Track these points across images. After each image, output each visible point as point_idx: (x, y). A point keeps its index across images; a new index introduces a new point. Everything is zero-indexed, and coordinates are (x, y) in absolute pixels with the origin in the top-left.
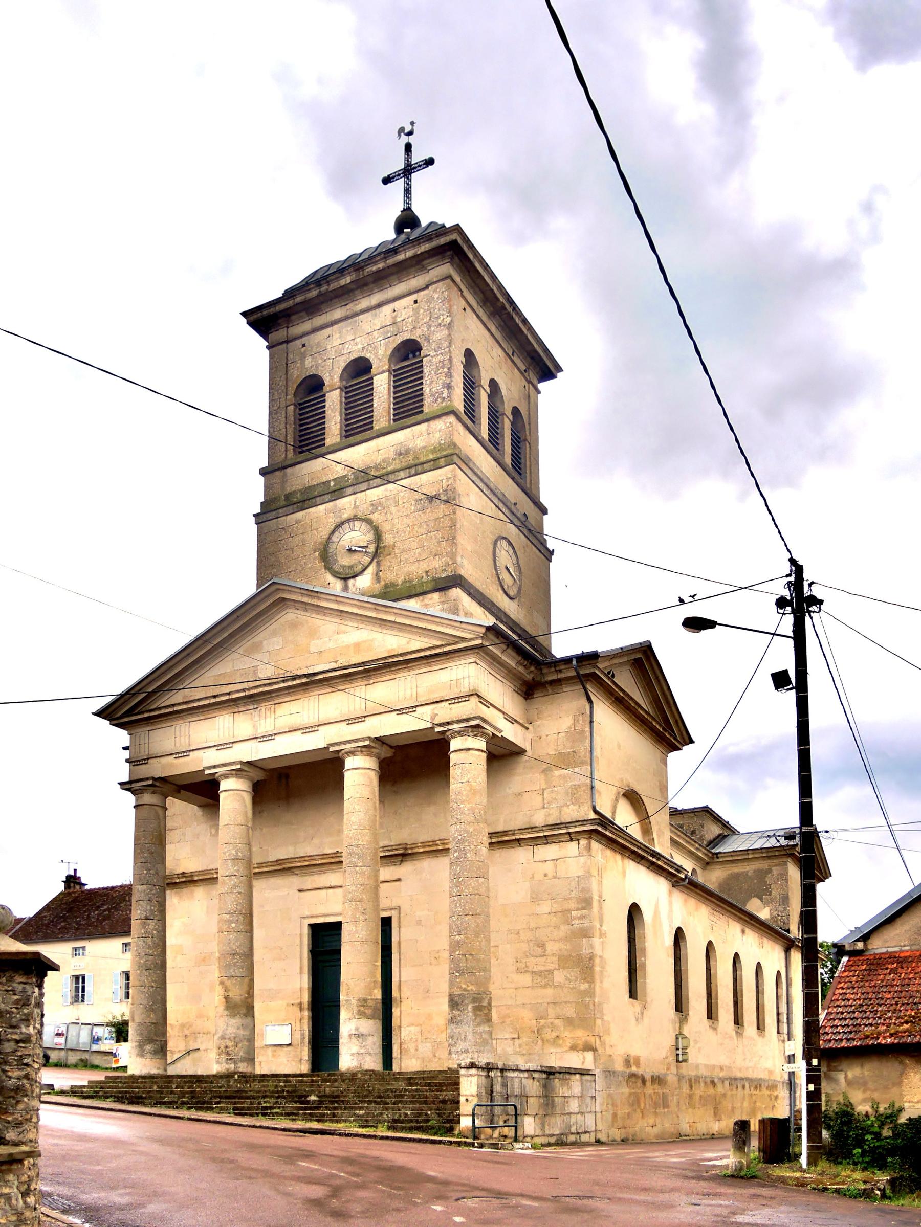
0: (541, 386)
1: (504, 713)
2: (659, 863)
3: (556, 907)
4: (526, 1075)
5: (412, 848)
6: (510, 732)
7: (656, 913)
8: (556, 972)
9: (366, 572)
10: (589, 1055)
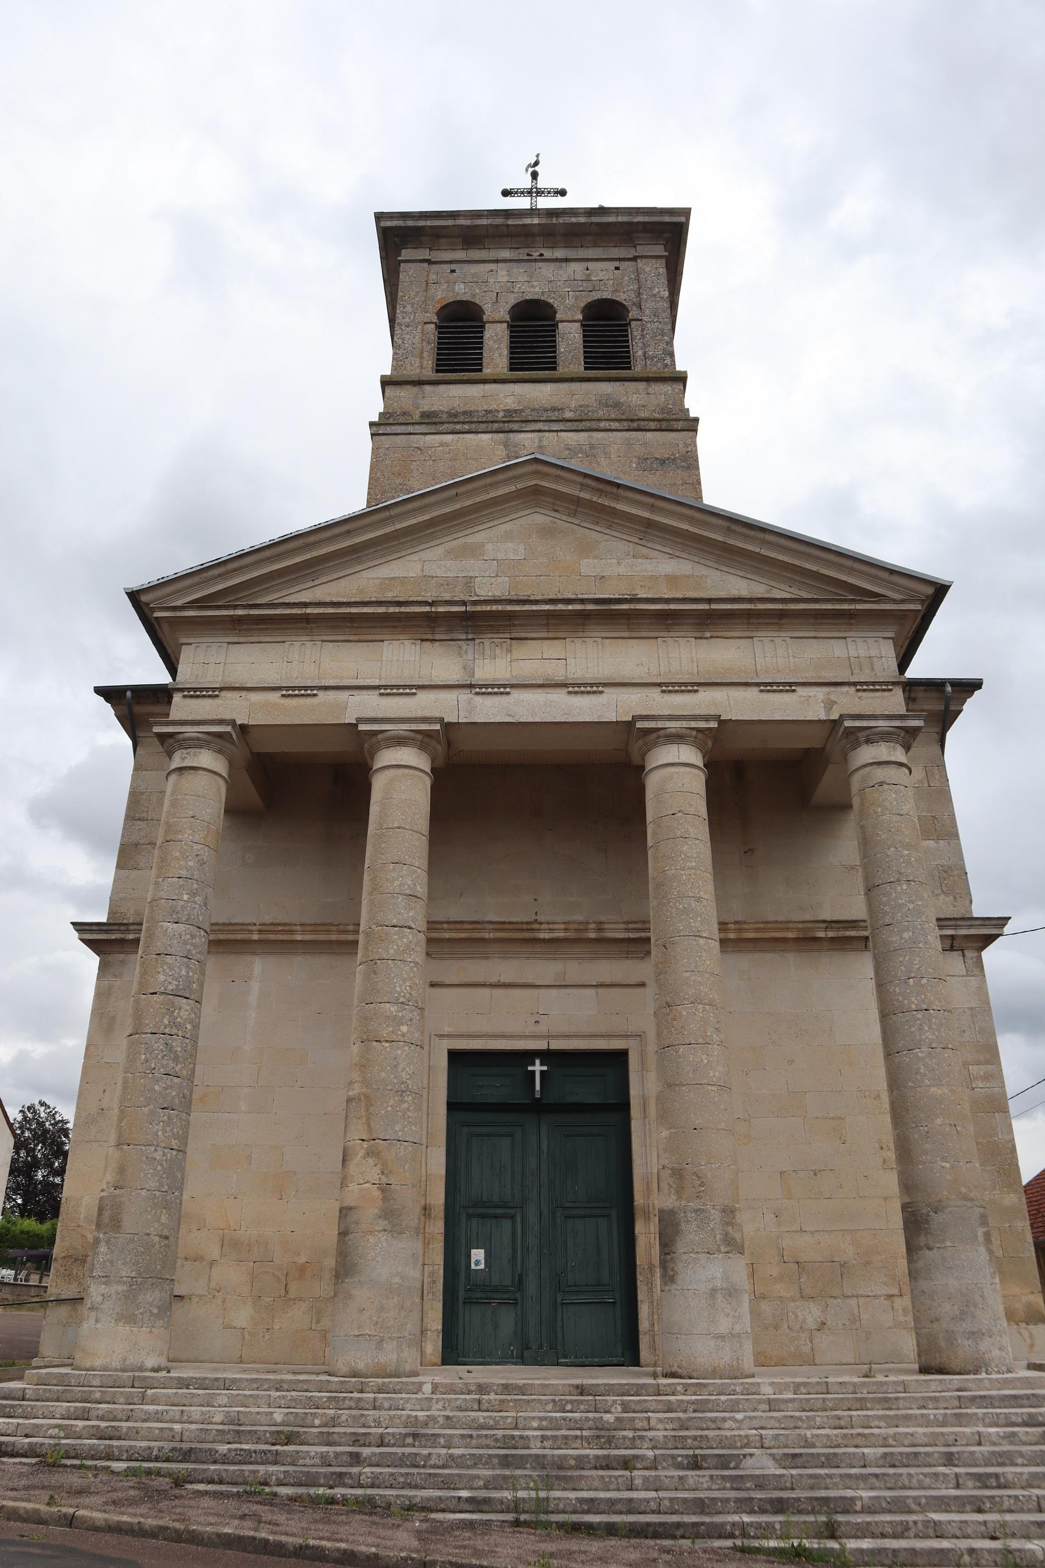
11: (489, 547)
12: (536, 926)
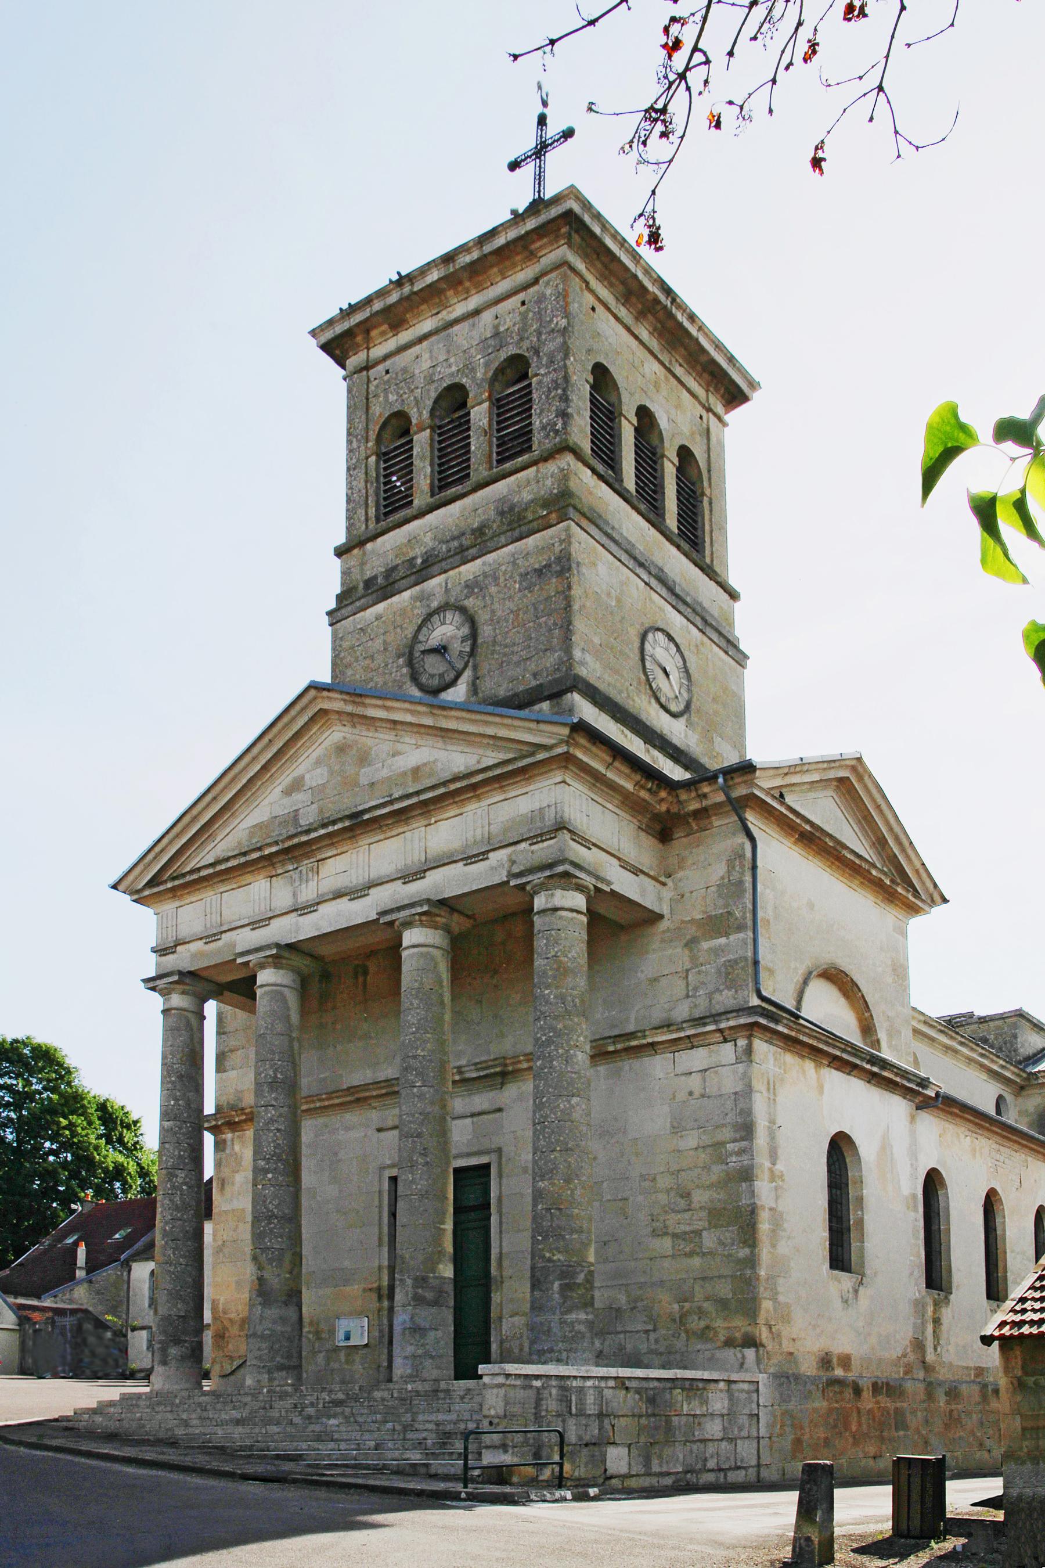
0: (730, 417)
1: (619, 859)
2: (886, 1074)
3: (707, 1140)
5: (514, 1063)
6: (625, 884)
7: (885, 1147)
8: (705, 1234)
9: (460, 681)
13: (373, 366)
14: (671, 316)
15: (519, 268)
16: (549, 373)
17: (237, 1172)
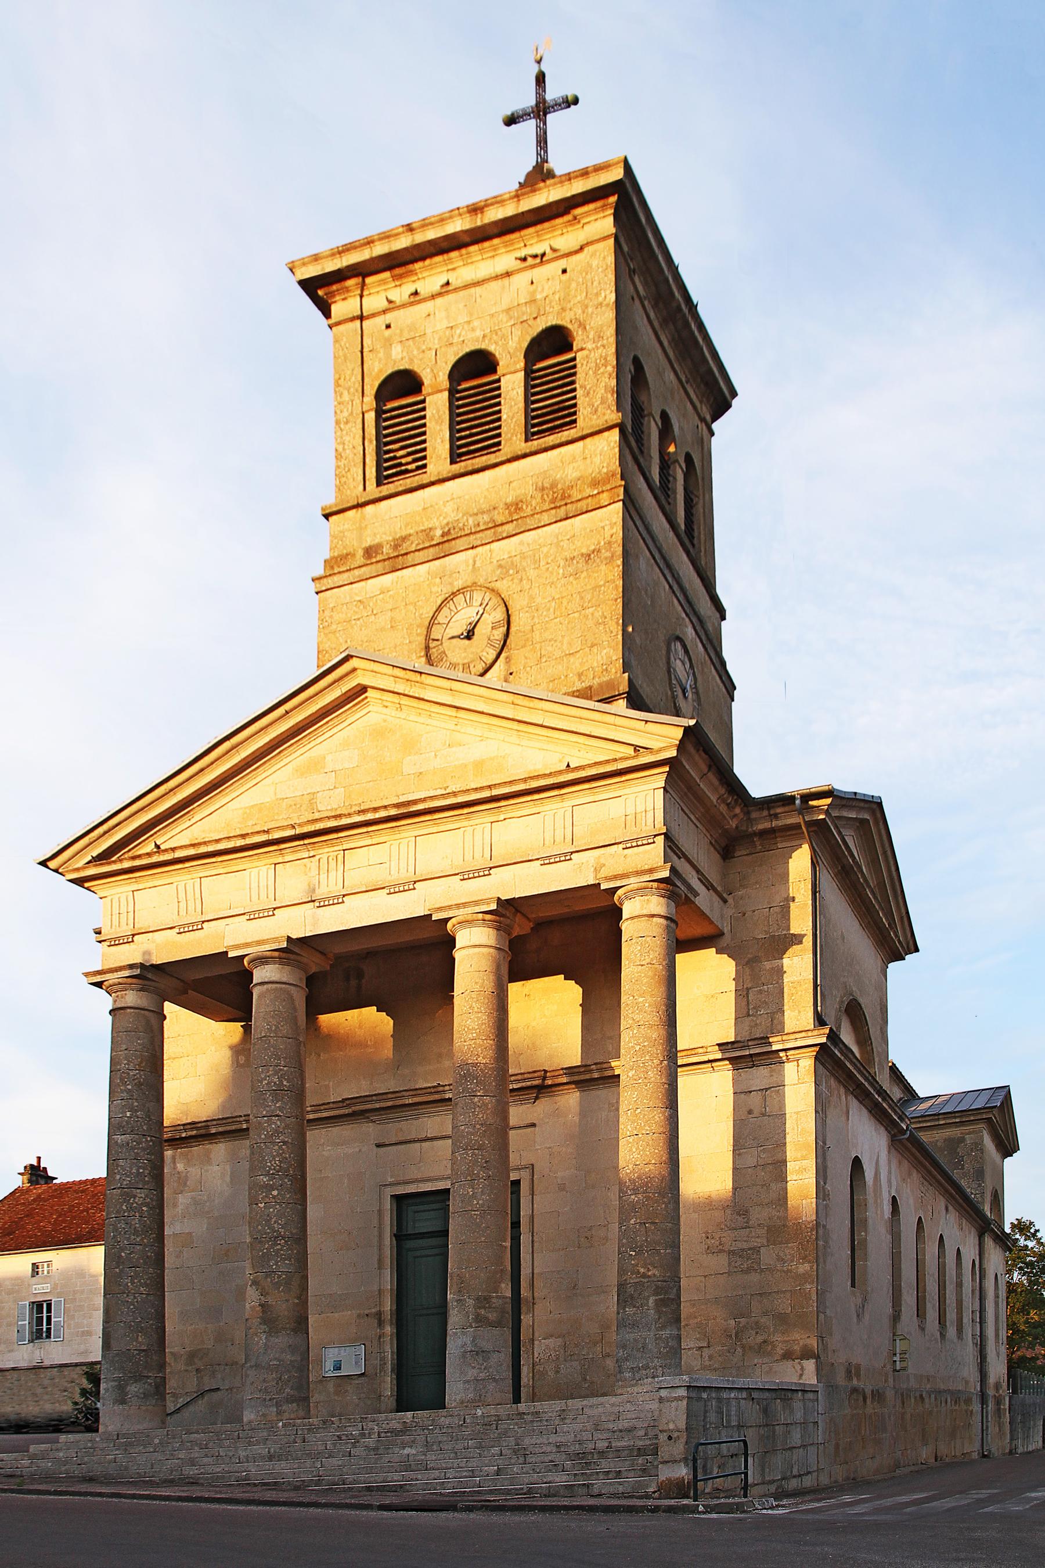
4: (744, 1395)
10: (810, 1365)
11: (329, 758)
12: (441, 1089)
13: (368, 317)
14: (687, 325)
15: (560, 232)
16: (598, 348)
17: (181, 1192)
